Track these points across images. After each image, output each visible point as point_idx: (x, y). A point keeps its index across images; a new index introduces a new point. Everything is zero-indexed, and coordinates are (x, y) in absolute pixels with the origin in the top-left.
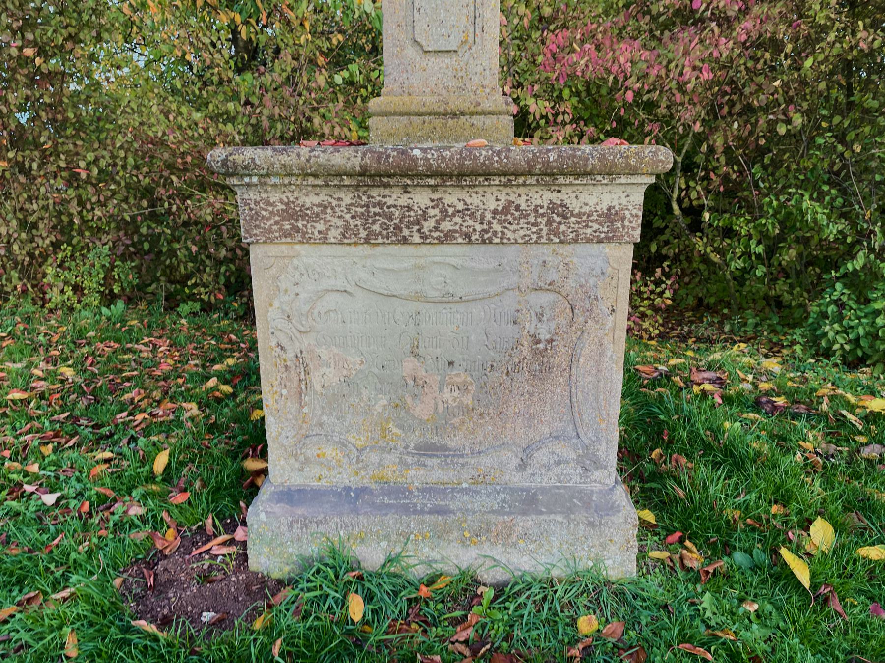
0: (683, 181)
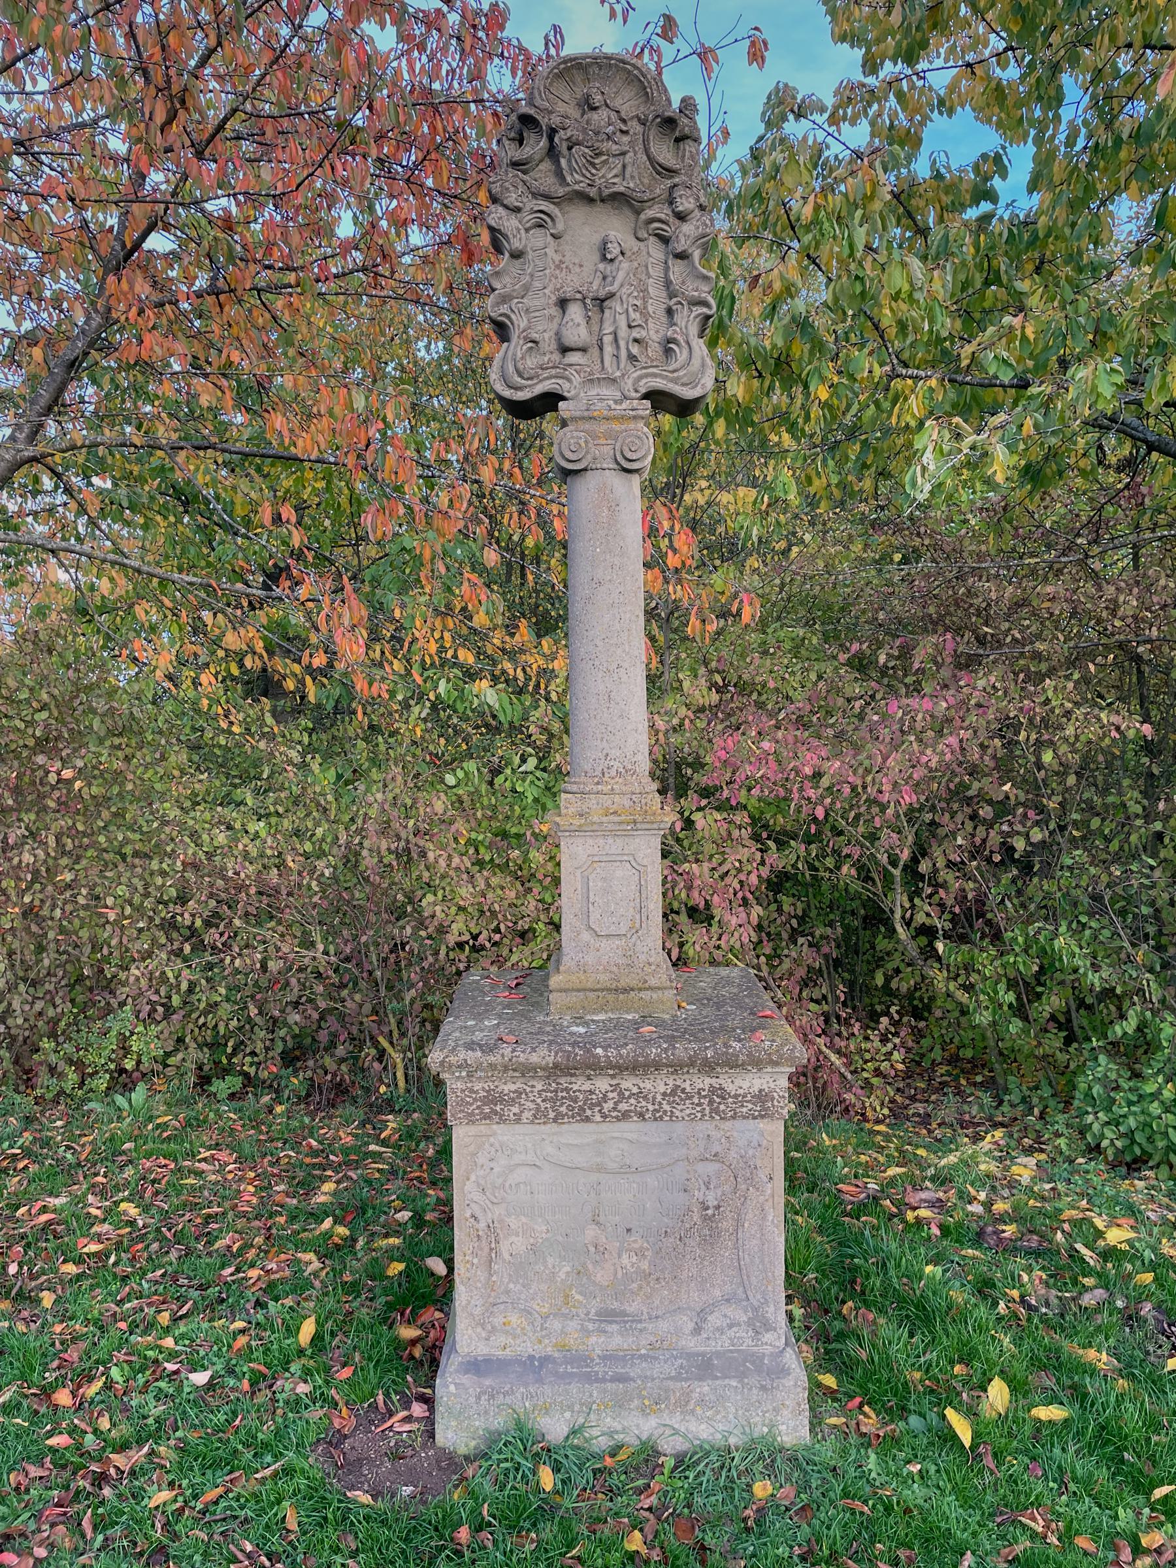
0: (905, 898)
